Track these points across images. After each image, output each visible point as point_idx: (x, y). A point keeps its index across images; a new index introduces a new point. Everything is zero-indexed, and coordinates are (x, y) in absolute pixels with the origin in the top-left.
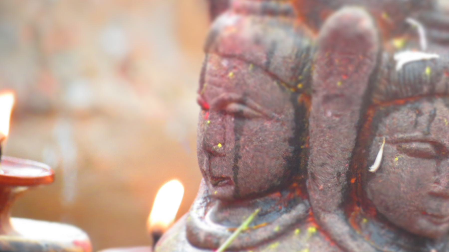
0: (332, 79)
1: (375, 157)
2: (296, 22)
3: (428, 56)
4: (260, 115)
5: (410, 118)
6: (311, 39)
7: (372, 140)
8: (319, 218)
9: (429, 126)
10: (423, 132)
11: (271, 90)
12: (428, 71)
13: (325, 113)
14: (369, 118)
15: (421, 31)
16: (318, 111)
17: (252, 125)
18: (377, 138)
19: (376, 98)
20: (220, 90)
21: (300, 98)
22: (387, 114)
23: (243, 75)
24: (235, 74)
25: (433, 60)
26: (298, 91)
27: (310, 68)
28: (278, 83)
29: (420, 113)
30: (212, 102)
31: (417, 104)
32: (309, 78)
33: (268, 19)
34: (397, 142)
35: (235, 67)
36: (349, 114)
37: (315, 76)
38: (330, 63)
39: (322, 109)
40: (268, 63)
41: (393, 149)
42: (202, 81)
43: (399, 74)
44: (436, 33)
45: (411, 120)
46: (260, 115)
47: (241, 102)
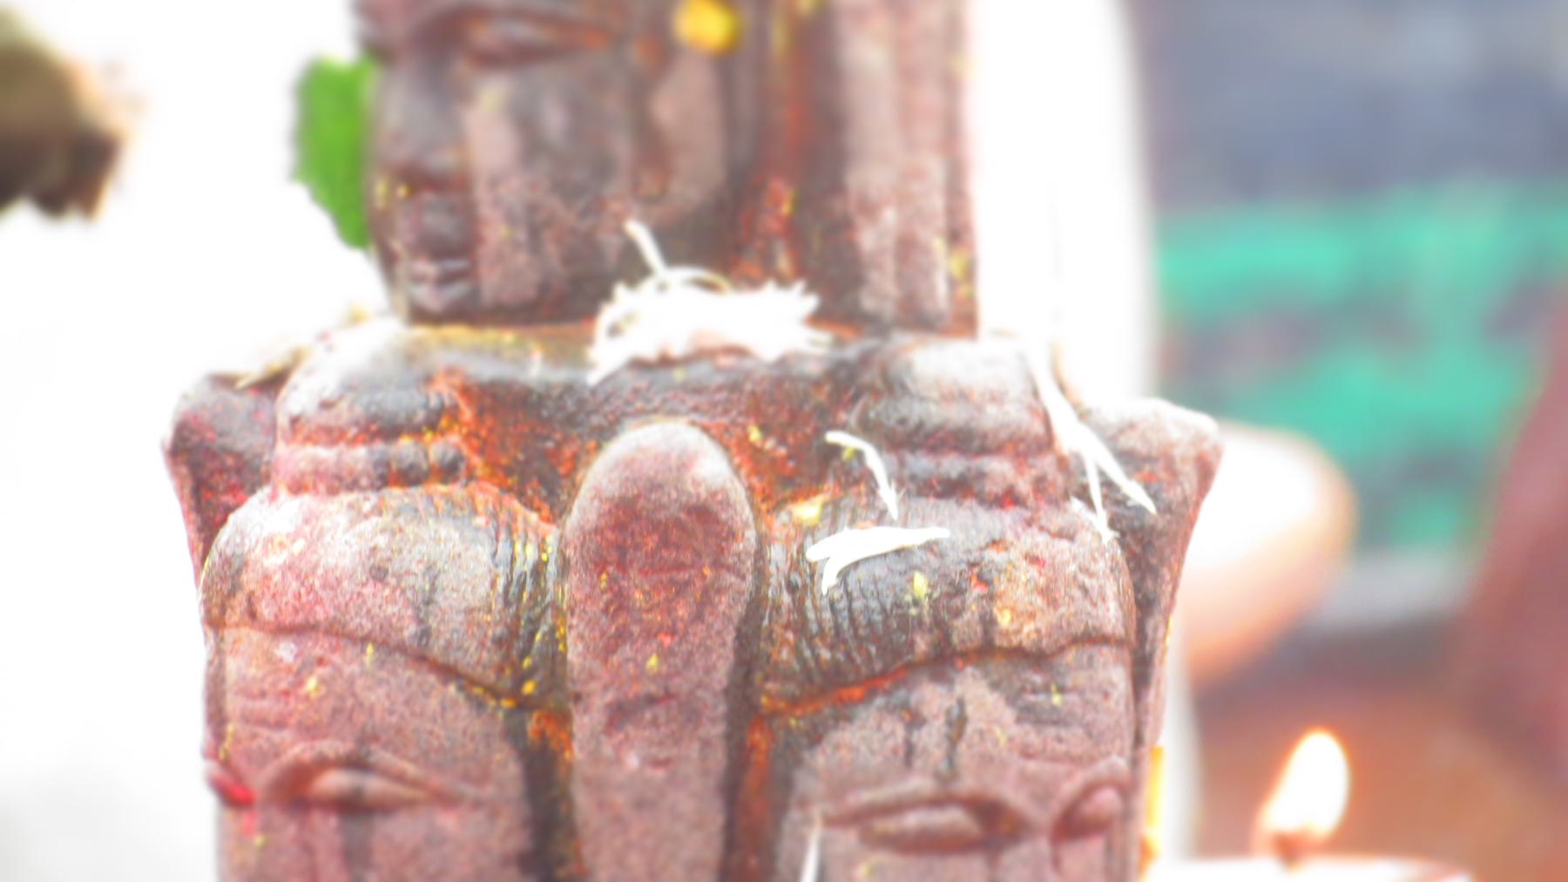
0: (627, 650)
2: (486, 494)
3: (913, 537)
5: (886, 738)
6: (540, 541)
7: (777, 825)
9: (951, 757)
10: (937, 775)
11: (448, 718)
12: (920, 584)
13: (618, 761)
14: (755, 757)
15: (876, 462)
16: (595, 756)
17: (400, 831)
18: (794, 815)
19: (770, 692)
20: (286, 735)
21: (532, 724)
23: (351, 682)
24: (322, 681)
25: (929, 547)
26: (524, 705)
27: (553, 629)
28: (461, 688)
29: (915, 721)
30: (260, 779)
31: (901, 694)
32: (554, 660)
33: (395, 496)
34: (860, 818)
35: (321, 661)
36: (694, 750)
37: (574, 653)
38: (619, 603)
39: (608, 750)
40: (425, 634)
41: (848, 839)
42: (216, 718)
44: (921, 463)
45: (890, 743)
47: (355, 763)
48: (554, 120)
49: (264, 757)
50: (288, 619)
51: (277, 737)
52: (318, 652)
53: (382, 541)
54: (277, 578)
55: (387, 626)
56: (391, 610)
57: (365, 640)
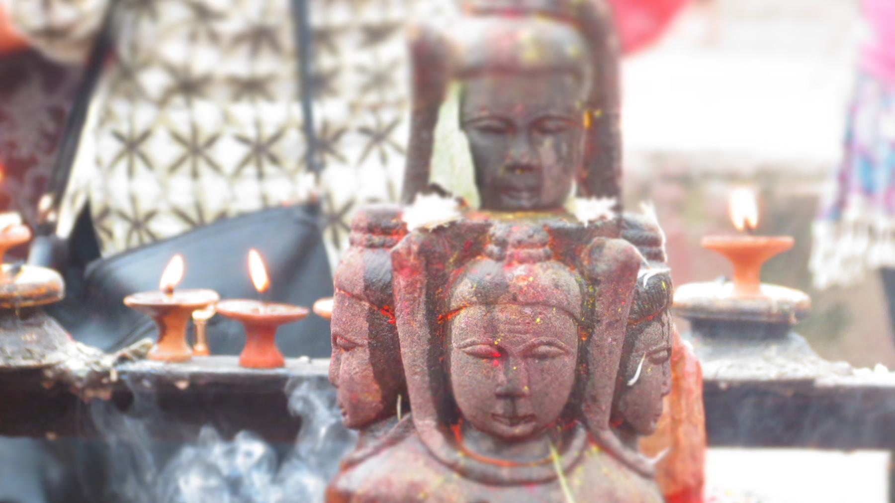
1: (635, 372)
4: (561, 351)
22: (641, 331)
23: (550, 319)
35: (540, 313)
46: (561, 351)
48: (564, 148)
49: (518, 343)
50: (529, 301)
51: (524, 336)
52: (539, 310)
53: (554, 276)
54: (525, 289)
55: (560, 303)
57: (553, 306)
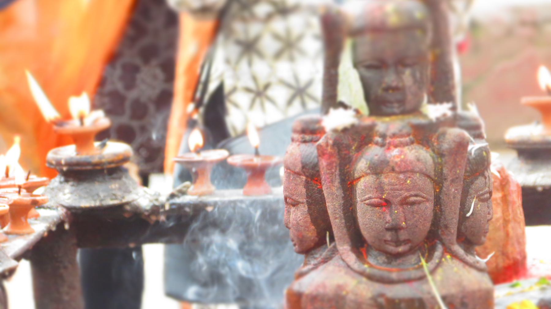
8: (450, 250)
22: (472, 183)
23: (416, 180)
35: (409, 177)
43: (474, 159)
48: (418, 75)
50: (402, 170)
51: (400, 192)
52: (408, 175)
56: (421, 166)
